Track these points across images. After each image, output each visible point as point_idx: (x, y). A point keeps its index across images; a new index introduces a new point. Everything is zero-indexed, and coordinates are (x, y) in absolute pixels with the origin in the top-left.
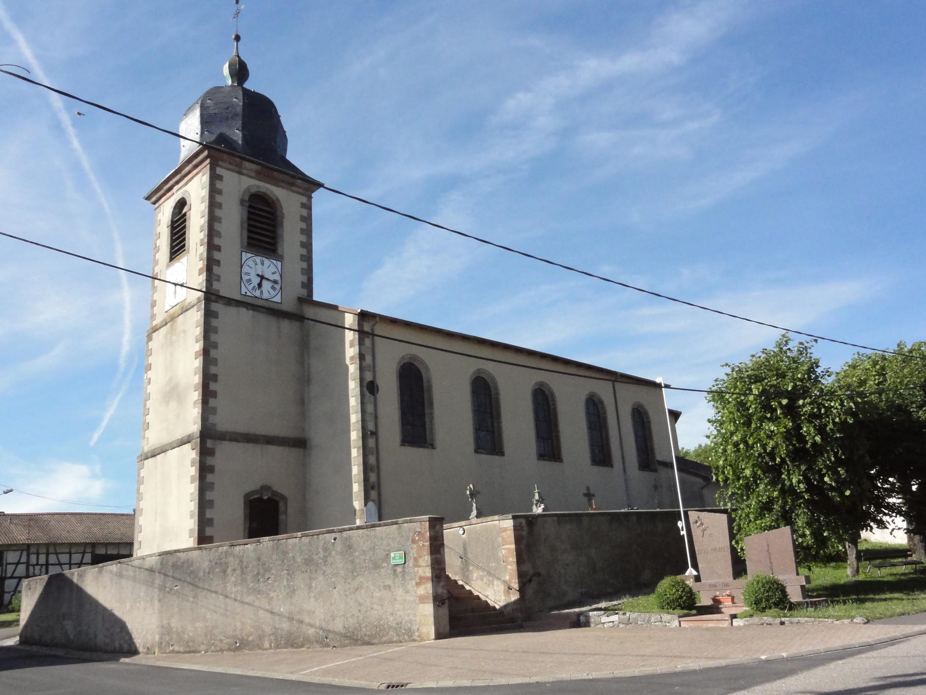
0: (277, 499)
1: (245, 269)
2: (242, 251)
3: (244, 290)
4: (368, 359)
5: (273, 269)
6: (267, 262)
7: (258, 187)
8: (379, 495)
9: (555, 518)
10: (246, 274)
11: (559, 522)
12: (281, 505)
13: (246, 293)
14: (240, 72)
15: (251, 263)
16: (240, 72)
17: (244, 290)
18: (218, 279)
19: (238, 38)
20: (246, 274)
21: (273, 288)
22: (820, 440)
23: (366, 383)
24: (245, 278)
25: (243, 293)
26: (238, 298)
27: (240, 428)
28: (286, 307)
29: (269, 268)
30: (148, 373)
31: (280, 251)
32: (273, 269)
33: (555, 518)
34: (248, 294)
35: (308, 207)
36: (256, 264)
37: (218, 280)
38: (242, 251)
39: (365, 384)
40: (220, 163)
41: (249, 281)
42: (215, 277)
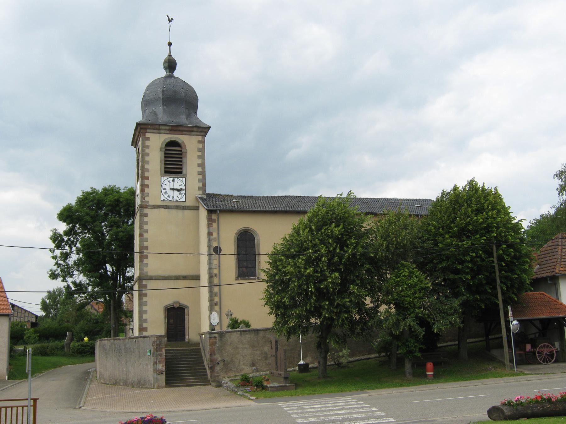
0: (184, 308)
1: (163, 186)
2: (161, 177)
3: (163, 198)
4: (215, 235)
5: (180, 183)
6: (176, 180)
7: (170, 138)
8: (220, 308)
9: (239, 333)
10: (164, 189)
11: (241, 334)
12: (186, 310)
13: (164, 199)
14: (170, 65)
15: (166, 182)
16: (170, 65)
17: (163, 198)
18: (148, 195)
19: (170, 44)
20: (164, 189)
21: (181, 194)
22: (505, 257)
23: (213, 248)
24: (163, 191)
25: (162, 200)
26: (160, 203)
27: (161, 273)
28: (188, 204)
29: (178, 182)
30: (8, 298)
31: (184, 172)
32: (180, 183)
33: (239, 333)
34: (166, 200)
35: (203, 142)
36: (170, 182)
37: (148, 196)
38: (161, 177)
39: (212, 249)
40: (148, 130)
41: (166, 193)
42: (146, 195)
